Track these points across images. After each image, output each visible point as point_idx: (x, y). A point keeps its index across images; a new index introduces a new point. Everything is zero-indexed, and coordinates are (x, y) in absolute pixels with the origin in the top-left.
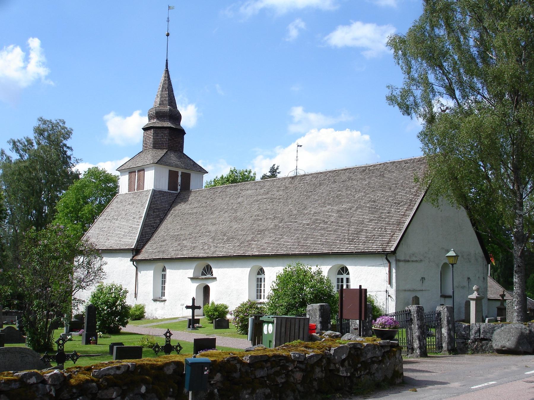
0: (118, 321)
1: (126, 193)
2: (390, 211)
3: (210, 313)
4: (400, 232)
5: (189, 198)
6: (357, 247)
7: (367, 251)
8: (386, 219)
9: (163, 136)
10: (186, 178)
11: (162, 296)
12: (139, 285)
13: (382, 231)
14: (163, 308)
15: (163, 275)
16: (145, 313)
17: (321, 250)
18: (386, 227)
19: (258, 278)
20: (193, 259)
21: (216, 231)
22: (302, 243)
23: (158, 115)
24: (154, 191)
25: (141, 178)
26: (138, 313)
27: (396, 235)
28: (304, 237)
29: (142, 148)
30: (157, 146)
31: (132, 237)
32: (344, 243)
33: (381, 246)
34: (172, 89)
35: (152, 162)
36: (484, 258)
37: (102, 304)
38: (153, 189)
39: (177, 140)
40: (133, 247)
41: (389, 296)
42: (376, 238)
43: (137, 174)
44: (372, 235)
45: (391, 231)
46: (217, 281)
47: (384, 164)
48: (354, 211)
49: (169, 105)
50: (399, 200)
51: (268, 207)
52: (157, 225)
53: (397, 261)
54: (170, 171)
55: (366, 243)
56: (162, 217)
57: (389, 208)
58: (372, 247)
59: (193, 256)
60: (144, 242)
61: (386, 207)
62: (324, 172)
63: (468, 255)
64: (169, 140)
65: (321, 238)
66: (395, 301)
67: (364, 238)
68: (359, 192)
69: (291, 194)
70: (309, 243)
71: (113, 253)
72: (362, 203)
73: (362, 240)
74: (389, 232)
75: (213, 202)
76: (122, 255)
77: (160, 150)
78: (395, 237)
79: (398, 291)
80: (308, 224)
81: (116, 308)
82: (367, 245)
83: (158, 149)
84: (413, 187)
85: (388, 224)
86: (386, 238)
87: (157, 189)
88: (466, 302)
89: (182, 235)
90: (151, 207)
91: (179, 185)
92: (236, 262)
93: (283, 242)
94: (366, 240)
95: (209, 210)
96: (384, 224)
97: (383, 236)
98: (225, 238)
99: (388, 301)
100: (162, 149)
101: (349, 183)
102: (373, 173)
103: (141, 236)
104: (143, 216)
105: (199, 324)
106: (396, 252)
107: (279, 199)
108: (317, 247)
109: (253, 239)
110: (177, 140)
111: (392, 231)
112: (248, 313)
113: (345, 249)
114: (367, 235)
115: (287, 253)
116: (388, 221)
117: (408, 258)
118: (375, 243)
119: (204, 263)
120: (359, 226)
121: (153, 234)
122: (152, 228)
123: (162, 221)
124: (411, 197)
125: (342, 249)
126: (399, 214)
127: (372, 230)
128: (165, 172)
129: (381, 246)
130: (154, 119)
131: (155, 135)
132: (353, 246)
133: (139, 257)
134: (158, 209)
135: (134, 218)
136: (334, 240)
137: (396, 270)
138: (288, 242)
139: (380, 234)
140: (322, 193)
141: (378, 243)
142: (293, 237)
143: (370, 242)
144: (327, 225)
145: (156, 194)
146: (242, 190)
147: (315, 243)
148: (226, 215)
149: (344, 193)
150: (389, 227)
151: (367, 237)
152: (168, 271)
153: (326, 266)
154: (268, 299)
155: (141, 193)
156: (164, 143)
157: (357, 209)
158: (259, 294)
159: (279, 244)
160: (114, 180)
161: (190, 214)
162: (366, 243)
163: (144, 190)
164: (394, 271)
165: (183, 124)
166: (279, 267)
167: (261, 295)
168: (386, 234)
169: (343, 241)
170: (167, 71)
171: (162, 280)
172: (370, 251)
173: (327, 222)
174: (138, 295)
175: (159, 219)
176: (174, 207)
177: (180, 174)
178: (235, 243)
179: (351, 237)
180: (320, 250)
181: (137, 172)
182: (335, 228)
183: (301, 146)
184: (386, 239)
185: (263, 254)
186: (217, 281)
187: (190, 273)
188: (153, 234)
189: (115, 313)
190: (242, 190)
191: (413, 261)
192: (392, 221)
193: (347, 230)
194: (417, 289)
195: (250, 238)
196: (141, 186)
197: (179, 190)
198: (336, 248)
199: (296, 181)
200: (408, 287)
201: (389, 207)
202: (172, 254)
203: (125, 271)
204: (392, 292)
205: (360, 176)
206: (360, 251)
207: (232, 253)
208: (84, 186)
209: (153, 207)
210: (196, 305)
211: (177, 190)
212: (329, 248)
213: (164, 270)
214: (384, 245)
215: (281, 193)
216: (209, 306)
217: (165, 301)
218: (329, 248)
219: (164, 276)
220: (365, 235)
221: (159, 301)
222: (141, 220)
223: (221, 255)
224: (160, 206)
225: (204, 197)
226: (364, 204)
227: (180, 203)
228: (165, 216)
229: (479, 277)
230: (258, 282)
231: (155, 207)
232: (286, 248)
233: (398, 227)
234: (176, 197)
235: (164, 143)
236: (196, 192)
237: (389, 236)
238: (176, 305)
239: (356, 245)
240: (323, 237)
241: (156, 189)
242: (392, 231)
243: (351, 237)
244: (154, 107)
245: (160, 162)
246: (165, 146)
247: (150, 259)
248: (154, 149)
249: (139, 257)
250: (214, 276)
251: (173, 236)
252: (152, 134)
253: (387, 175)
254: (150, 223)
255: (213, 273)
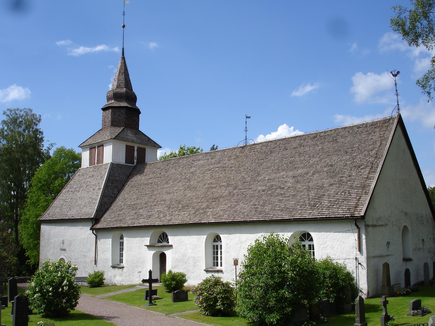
0: (65, 303)
1: (88, 167)
2: (351, 175)
3: (167, 283)
4: (367, 195)
5: (144, 170)
6: (321, 213)
7: (333, 216)
8: (348, 183)
9: (121, 115)
10: (142, 152)
11: (120, 263)
12: (99, 253)
13: (346, 195)
14: (121, 275)
15: (121, 242)
16: (104, 279)
17: (281, 216)
18: (350, 191)
19: (214, 246)
20: (150, 228)
21: (171, 200)
22: (260, 209)
23: (116, 96)
24: (112, 164)
25: (101, 153)
26: (97, 280)
27: (362, 199)
28: (261, 203)
29: (102, 126)
30: (115, 124)
31: (92, 207)
32: (305, 208)
33: (348, 211)
34: (128, 72)
35: (110, 137)
36: (433, 219)
37: (47, 284)
38: (111, 163)
39: (133, 118)
40: (92, 217)
41: (359, 264)
42: (340, 202)
43: (96, 149)
44: (336, 199)
45: (356, 194)
46: (173, 248)
47: (335, 130)
48: (310, 176)
49: (125, 87)
50: (359, 163)
51: (221, 175)
52: (115, 195)
53: (367, 226)
54: (127, 146)
55: (331, 208)
56: (120, 188)
57: (349, 172)
58: (338, 212)
59: (149, 224)
60: (103, 211)
61: (345, 171)
62: (274, 141)
63: (421, 217)
64: (125, 118)
65: (279, 203)
66: (366, 269)
67: (327, 203)
68: (313, 157)
69: (242, 162)
70: (267, 209)
71: (75, 222)
72: (318, 167)
73: (325, 205)
74: (354, 196)
75: (166, 172)
76: (82, 223)
77: (117, 127)
78: (363, 201)
79: (368, 258)
80: (263, 191)
81: (63, 289)
82: (332, 210)
83: (116, 126)
84: (372, 150)
85: (351, 187)
86: (351, 202)
87: (114, 163)
88: (425, 265)
89: (138, 204)
90: (110, 179)
91: (136, 159)
92: (192, 230)
93: (239, 209)
94: (330, 205)
95: (163, 180)
96: (347, 188)
97: (349, 200)
98: (180, 206)
99: (358, 269)
100: (119, 126)
101: (301, 150)
102: (325, 139)
103: (101, 206)
104: (102, 187)
105: (156, 295)
106: (365, 217)
107: (231, 167)
108: (276, 213)
109: (208, 207)
110: (133, 118)
111: (357, 194)
112: (212, 291)
113: (307, 215)
114: (330, 199)
115: (245, 220)
116: (350, 184)
117: (375, 223)
118: (340, 208)
119: (159, 231)
120: (319, 191)
121: (111, 204)
122: (110, 198)
123: (119, 191)
124: (371, 159)
125: (304, 215)
126: (361, 177)
127: (335, 194)
128: (122, 147)
129: (348, 211)
130: (112, 99)
131: (113, 114)
132: (316, 211)
133: (98, 226)
134: (116, 181)
135: (94, 190)
136: (294, 206)
137: (366, 236)
138: (245, 209)
139: (344, 199)
140: (274, 160)
141: (344, 208)
142: (249, 204)
143: (334, 206)
144: (284, 191)
145: (114, 167)
146: (194, 161)
147: (273, 209)
148: (180, 184)
149: (297, 159)
150: (353, 191)
151: (330, 202)
152: (125, 239)
153: (287, 233)
154: (240, 277)
155: (100, 166)
156: (121, 121)
157: (313, 174)
158: (216, 261)
159: (235, 211)
160: (77, 158)
161: (146, 184)
162: (331, 208)
163: (103, 164)
164: (364, 237)
165: (138, 105)
166: (236, 235)
167: (217, 263)
168: (351, 198)
169: (304, 206)
170: (123, 58)
171: (120, 247)
172: (336, 216)
173: (283, 188)
174: (98, 262)
175: (117, 189)
176: (131, 178)
177: (136, 149)
178: (190, 211)
179: (313, 203)
180: (280, 217)
181: (96, 147)
182: (293, 193)
183: (249, 117)
184: (353, 203)
185: (219, 221)
186: (173, 248)
187: (147, 241)
188: (111, 204)
189: (63, 294)
190: (194, 161)
191: (379, 226)
192: (355, 184)
193: (307, 195)
194: (385, 255)
195: (204, 205)
196: (100, 159)
197: (135, 163)
198: (298, 214)
199: (246, 151)
200: (377, 253)
201: (349, 170)
202: (129, 223)
203: (86, 239)
204: (363, 259)
205: (311, 142)
206: (325, 216)
207: (188, 220)
208: (55, 163)
209: (111, 179)
210: (154, 277)
211: (133, 163)
212: (290, 214)
213: (122, 238)
214: (351, 209)
215: (232, 162)
216: (166, 275)
217: (123, 268)
218: (290, 214)
219: (122, 244)
220: (328, 200)
221: (117, 267)
222: (100, 191)
223: (177, 223)
224: (118, 178)
225: (158, 168)
226: (320, 169)
227: (136, 174)
228: (123, 187)
229: (430, 238)
230: (214, 249)
231: (113, 179)
232: (244, 215)
233: (363, 190)
234: (133, 170)
235: (121, 121)
236: (151, 164)
237: (355, 200)
238: (133, 272)
239: (319, 211)
240: (281, 203)
241: (114, 162)
242: (357, 194)
243: (313, 203)
244: (112, 89)
245: (117, 138)
246: (122, 124)
247: (108, 228)
248: (112, 127)
249: (98, 226)
250: (170, 244)
251: (130, 206)
252: (111, 113)
253: (341, 140)
254: (108, 193)
255: (169, 240)
